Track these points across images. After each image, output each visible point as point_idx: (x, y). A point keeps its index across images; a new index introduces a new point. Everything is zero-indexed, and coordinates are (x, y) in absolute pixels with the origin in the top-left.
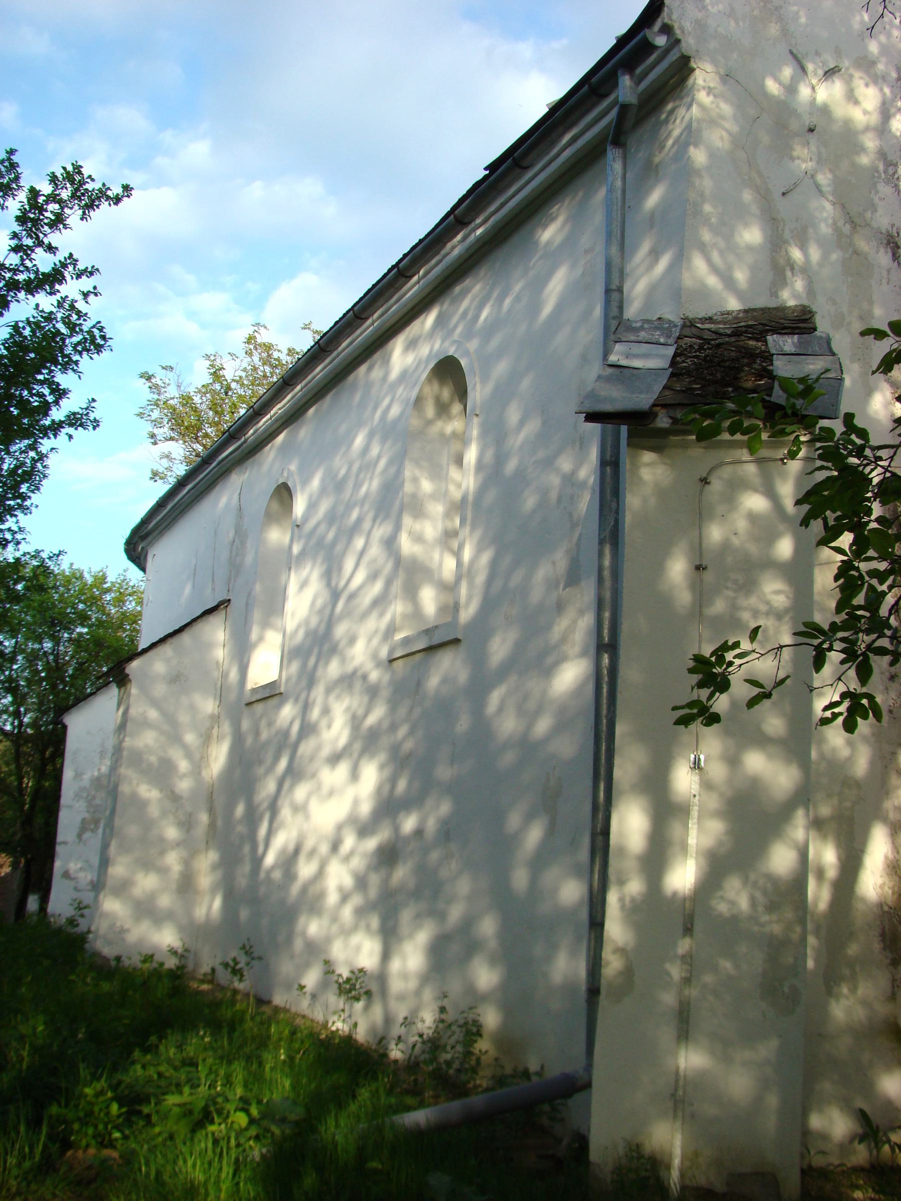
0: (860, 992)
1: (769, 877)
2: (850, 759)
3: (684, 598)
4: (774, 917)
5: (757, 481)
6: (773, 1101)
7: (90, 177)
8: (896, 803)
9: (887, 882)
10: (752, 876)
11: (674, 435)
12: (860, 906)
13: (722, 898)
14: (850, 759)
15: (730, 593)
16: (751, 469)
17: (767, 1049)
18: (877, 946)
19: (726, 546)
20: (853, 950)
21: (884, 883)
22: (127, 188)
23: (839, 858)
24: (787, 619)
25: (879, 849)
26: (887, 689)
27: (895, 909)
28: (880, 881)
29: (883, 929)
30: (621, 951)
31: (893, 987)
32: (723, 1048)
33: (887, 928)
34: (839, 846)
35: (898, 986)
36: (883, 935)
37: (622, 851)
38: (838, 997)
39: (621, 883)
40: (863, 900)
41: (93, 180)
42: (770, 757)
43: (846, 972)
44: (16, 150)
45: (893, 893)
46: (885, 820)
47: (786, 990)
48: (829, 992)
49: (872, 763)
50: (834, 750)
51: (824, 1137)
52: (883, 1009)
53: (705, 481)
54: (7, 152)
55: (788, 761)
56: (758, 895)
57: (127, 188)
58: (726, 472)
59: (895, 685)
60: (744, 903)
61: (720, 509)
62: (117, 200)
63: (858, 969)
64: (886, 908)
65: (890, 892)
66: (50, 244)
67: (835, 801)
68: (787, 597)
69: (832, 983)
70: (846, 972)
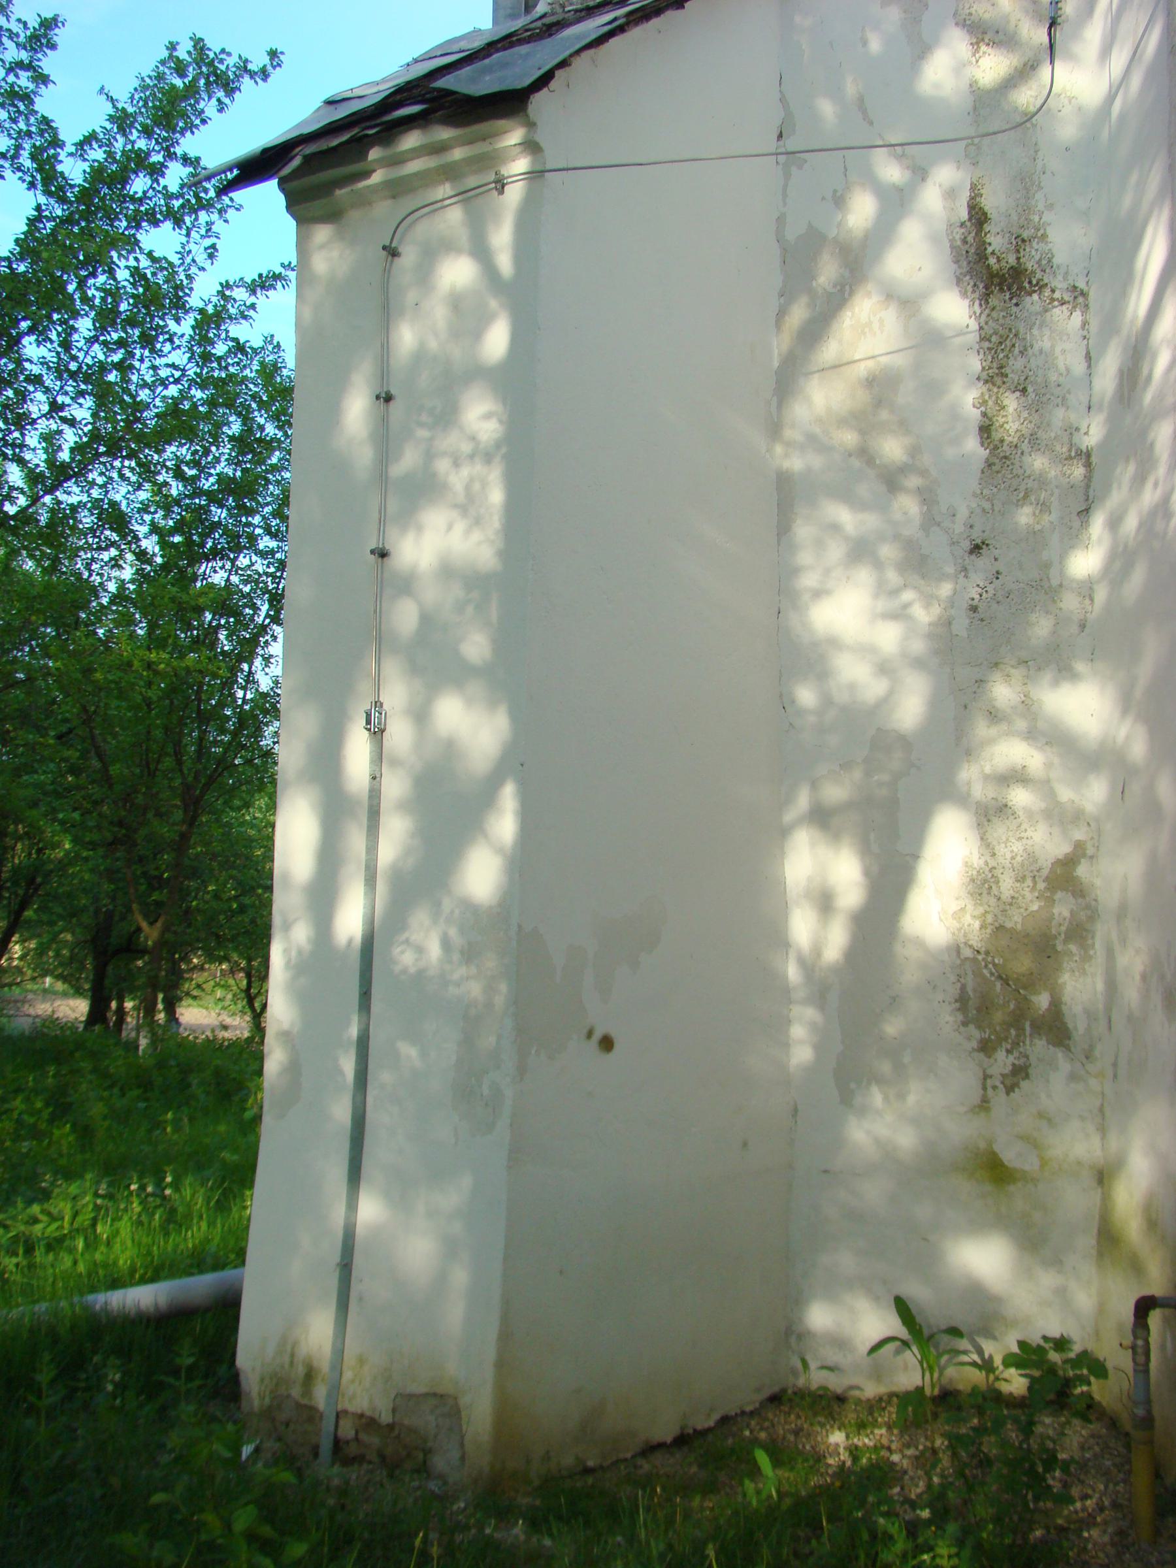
0: (911, 1099)
1: (469, 907)
2: (886, 701)
3: (364, 457)
4: (473, 970)
5: (463, 236)
6: (460, 1277)
7: (223, 51)
8: (988, 770)
9: (970, 907)
10: (447, 904)
11: (341, 188)
12: (906, 953)
13: (407, 941)
14: (886, 701)
15: (422, 433)
16: (455, 215)
17: (453, 1197)
18: (948, 1018)
19: (420, 356)
20: (892, 1028)
21: (963, 909)
22: (273, 54)
23: (867, 873)
24: (497, 459)
25: (949, 852)
26: (965, 569)
27: (987, 953)
28: (955, 906)
29: (963, 988)
30: (285, 1036)
31: (985, 1089)
32: (400, 1195)
33: (969, 989)
34: (865, 850)
35: (994, 1088)
36: (962, 1001)
37: (286, 877)
38: (862, 1112)
39: (287, 927)
40: (919, 942)
41: (229, 54)
42: (469, 702)
43: (886, 1067)
44: (178, 43)
45: (983, 927)
46: (961, 799)
47: (486, 1091)
48: (846, 1098)
49: (934, 704)
50: (852, 687)
51: (841, 1343)
52: (961, 1131)
53: (392, 253)
54: (168, 48)
55: (492, 705)
56: (453, 932)
57: (273, 54)
58: (423, 229)
59: (983, 562)
60: (434, 950)
61: (411, 296)
62: (264, 74)
63: (907, 1059)
64: (967, 953)
65: (977, 924)
66: (185, 154)
67: (857, 774)
68: (501, 422)
69: (853, 1085)
70: (886, 1067)
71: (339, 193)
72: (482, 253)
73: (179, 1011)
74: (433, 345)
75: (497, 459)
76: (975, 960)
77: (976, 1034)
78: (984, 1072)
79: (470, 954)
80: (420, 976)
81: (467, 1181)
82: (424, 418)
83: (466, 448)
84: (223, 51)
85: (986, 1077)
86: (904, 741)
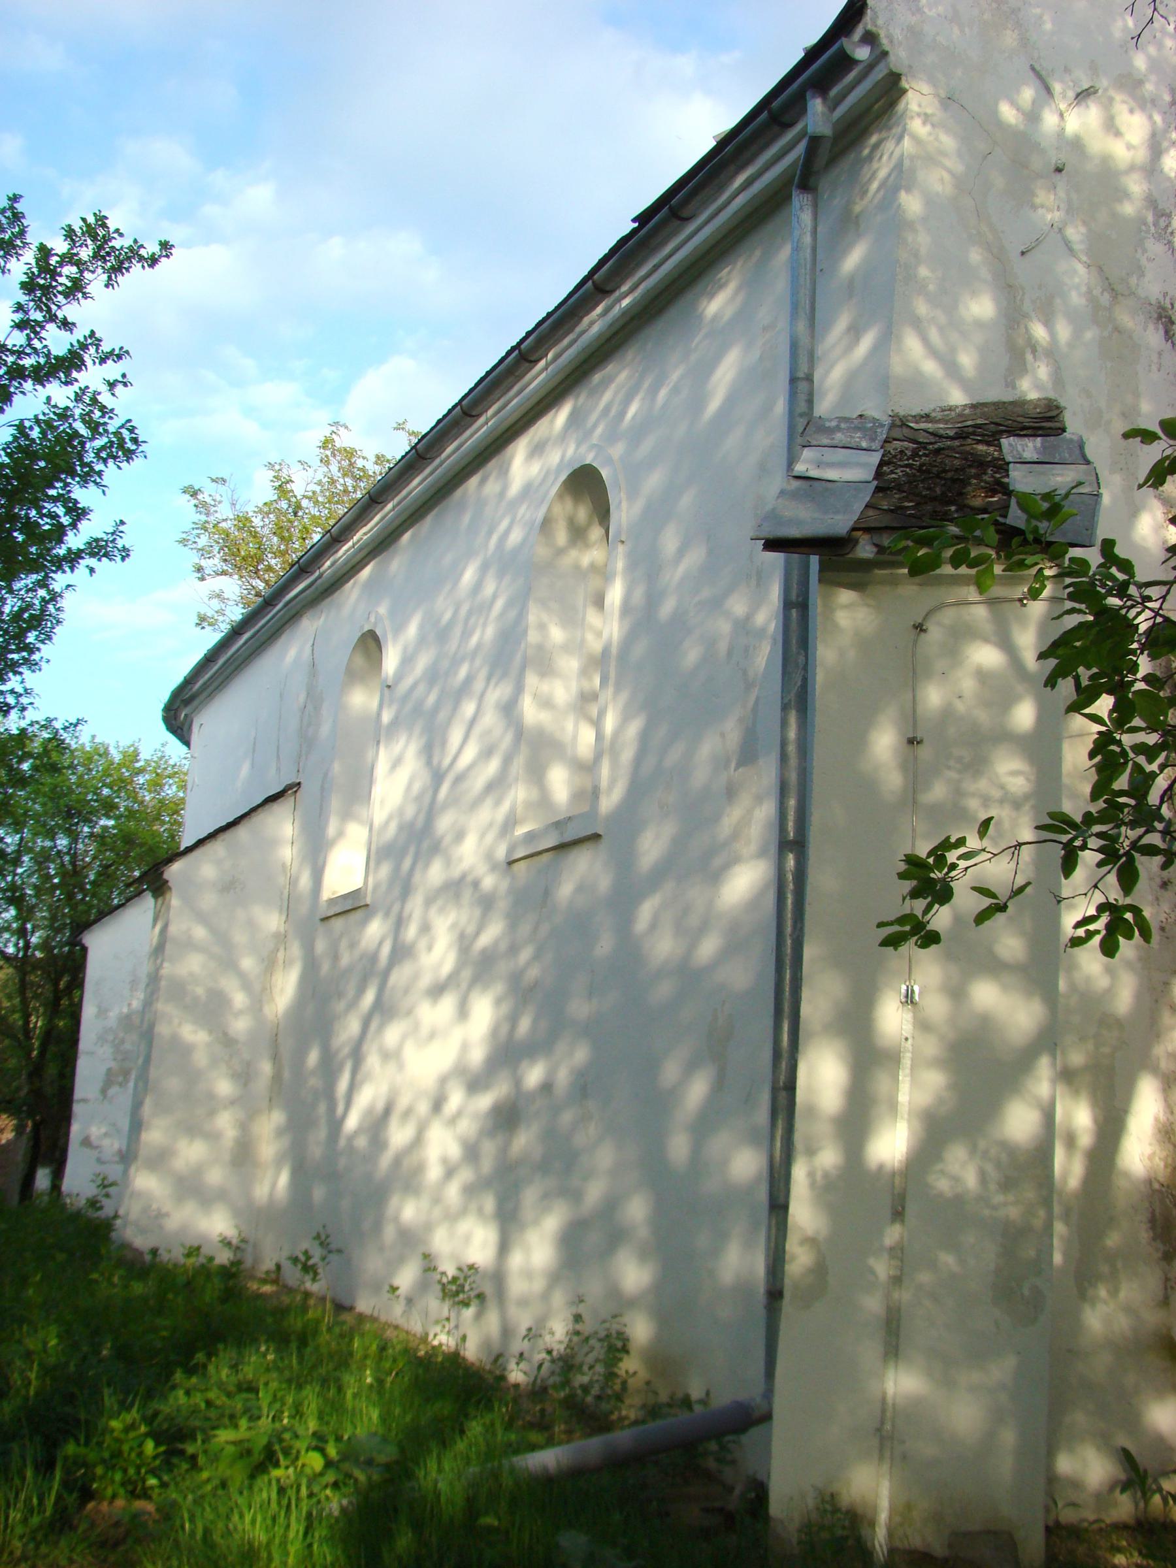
0: (1123, 1294)
2: (1110, 992)
3: (893, 781)
4: (1010, 1198)
5: (988, 628)
6: (1008, 1437)
8: (1170, 1049)
9: (1158, 1152)
10: (982, 1144)
11: (880, 569)
12: (1121, 1183)
14: (1110, 992)
15: (953, 775)
16: (980, 612)
18: (1144, 1235)
19: (947, 713)
20: (1113, 1240)
21: (1154, 1153)
22: (166, 246)
24: (1027, 808)
25: (1147, 1108)
27: (1168, 1187)
28: (1148, 1150)
29: (1153, 1213)
30: (810, 1241)
31: (1166, 1289)
36: (1152, 1221)
37: (811, 1110)
38: (1093, 1301)
39: (811, 1152)
40: (1126, 1175)
41: (121, 235)
42: (1005, 988)
43: (1105, 1269)
44: (21, 196)
45: (1166, 1166)
46: (1155, 1070)
47: (1026, 1292)
48: (1083, 1296)
49: (1138, 997)
50: (1088, 979)
51: (1076, 1484)
52: (1152, 1318)
53: (920, 628)
54: (9, 199)
56: (990, 1168)
57: (166, 246)
58: (948, 616)
62: (153, 261)
63: (1119, 1265)
64: (1156, 1186)
65: (1162, 1164)
66: (65, 318)
67: (1090, 1046)
68: (1028, 779)
71: (877, 571)
72: (1006, 644)
73: (132, 1170)
74: (960, 707)
75: (1027, 808)
76: (1160, 1191)
77: (1161, 1246)
78: (1166, 1275)
79: (1007, 1184)
80: (958, 1200)
81: (1010, 1362)
82: (952, 763)
83: (996, 793)
84: (117, 231)
85: (1167, 1279)
86: (1119, 1023)
